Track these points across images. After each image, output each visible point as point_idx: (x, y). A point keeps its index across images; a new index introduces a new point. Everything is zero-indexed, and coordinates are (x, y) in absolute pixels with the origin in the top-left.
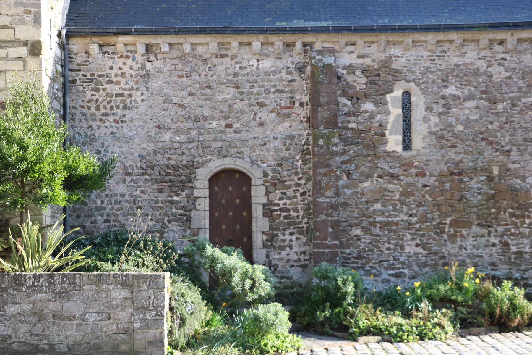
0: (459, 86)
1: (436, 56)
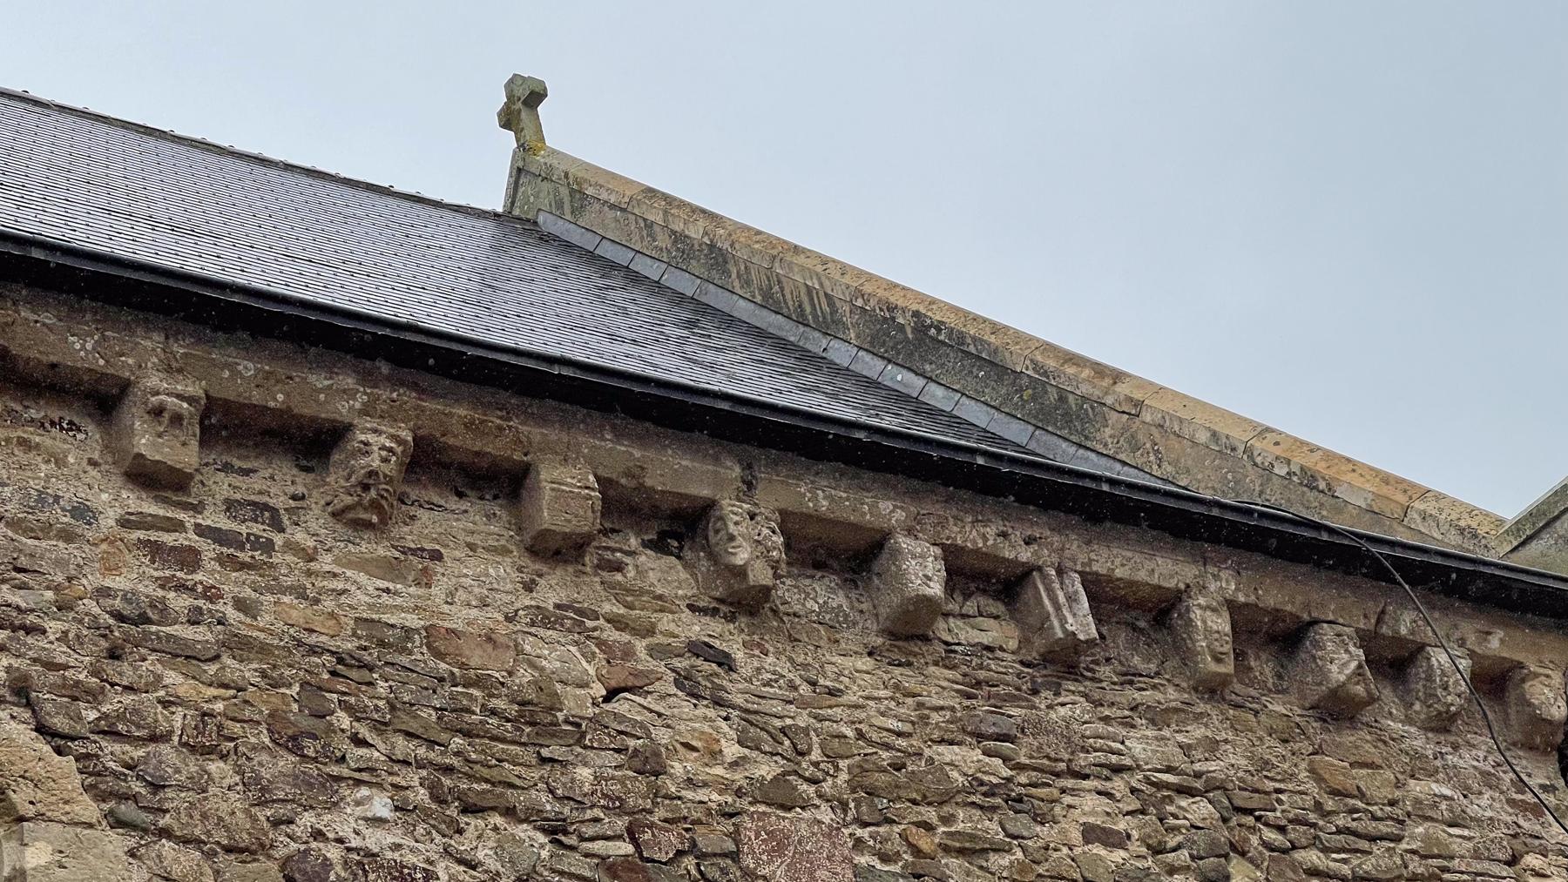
0: (422, 796)
1: (201, 531)
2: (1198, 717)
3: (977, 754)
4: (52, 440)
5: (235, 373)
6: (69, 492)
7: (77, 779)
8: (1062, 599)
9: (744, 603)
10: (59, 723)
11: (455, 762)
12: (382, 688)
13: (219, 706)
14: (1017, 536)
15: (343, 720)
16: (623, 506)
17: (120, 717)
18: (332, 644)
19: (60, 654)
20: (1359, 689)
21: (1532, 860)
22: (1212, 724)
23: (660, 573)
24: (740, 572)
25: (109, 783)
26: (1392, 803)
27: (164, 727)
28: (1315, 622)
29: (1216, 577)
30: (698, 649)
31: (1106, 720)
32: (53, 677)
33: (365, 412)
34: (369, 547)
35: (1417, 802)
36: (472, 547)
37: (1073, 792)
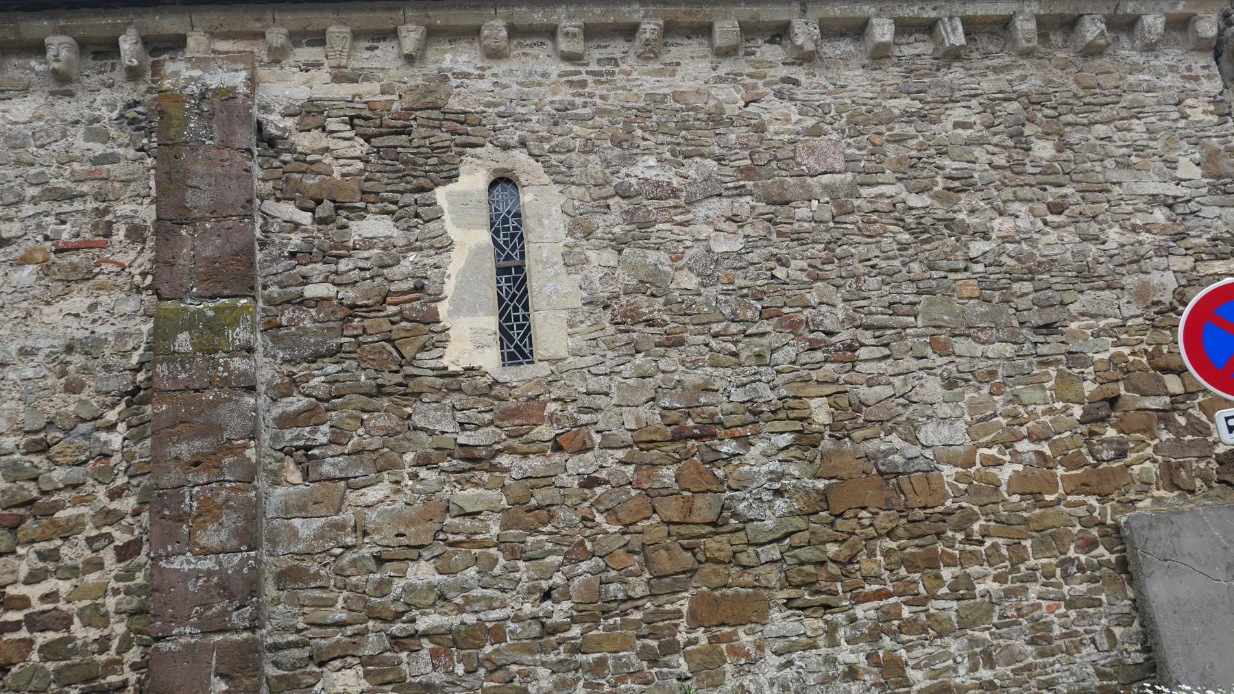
0: (668, 155)
2: (1019, 67)
3: (908, 100)
4: (535, 51)
5: (594, 14)
6: (540, 70)
7: (542, 170)
8: (949, 29)
9: (805, 59)
10: (536, 152)
11: (681, 141)
12: (655, 118)
13: (593, 136)
14: (928, 8)
15: (639, 132)
16: (749, 30)
17: (557, 146)
18: (636, 105)
19: (537, 127)
20: (1102, 41)
21: (1189, 102)
22: (1028, 65)
23: (769, 52)
24: (801, 47)
25: (553, 169)
26: (1117, 87)
27: (572, 147)
28: (1081, 16)
30: (786, 80)
31: (972, 76)
32: (534, 136)
33: (645, 16)
34: (654, 65)
35: (1131, 85)
36: (692, 58)
37: (951, 109)
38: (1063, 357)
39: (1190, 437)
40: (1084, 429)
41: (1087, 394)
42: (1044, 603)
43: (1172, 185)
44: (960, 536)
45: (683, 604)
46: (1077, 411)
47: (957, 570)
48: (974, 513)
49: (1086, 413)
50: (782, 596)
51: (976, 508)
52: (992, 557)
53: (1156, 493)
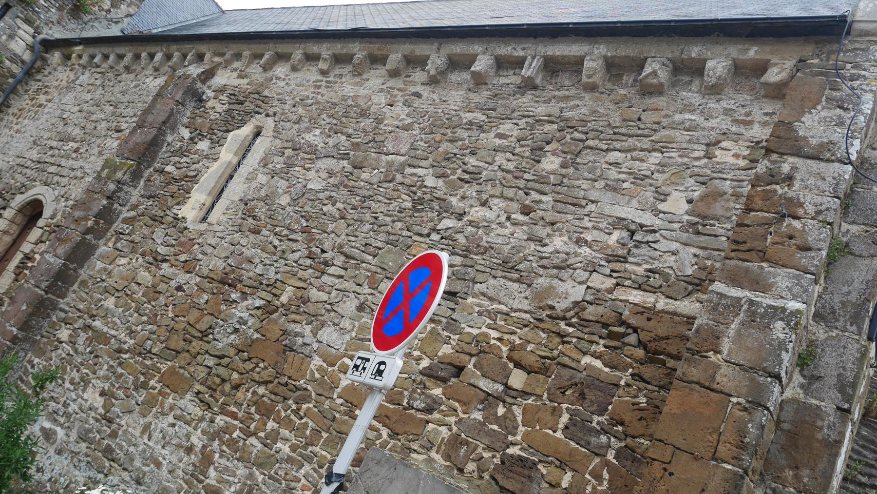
2: (579, 98)
14: (519, 49)
29: (598, 49)
34: (357, 80)
38: (444, 320)
39: (495, 427)
40: (420, 378)
41: (440, 354)
42: (303, 481)
43: (648, 214)
44: (294, 407)
45: (164, 368)
46: (425, 363)
47: (276, 426)
48: (310, 396)
49: (429, 368)
50: (198, 387)
51: (313, 394)
52: (299, 431)
53: (433, 454)
